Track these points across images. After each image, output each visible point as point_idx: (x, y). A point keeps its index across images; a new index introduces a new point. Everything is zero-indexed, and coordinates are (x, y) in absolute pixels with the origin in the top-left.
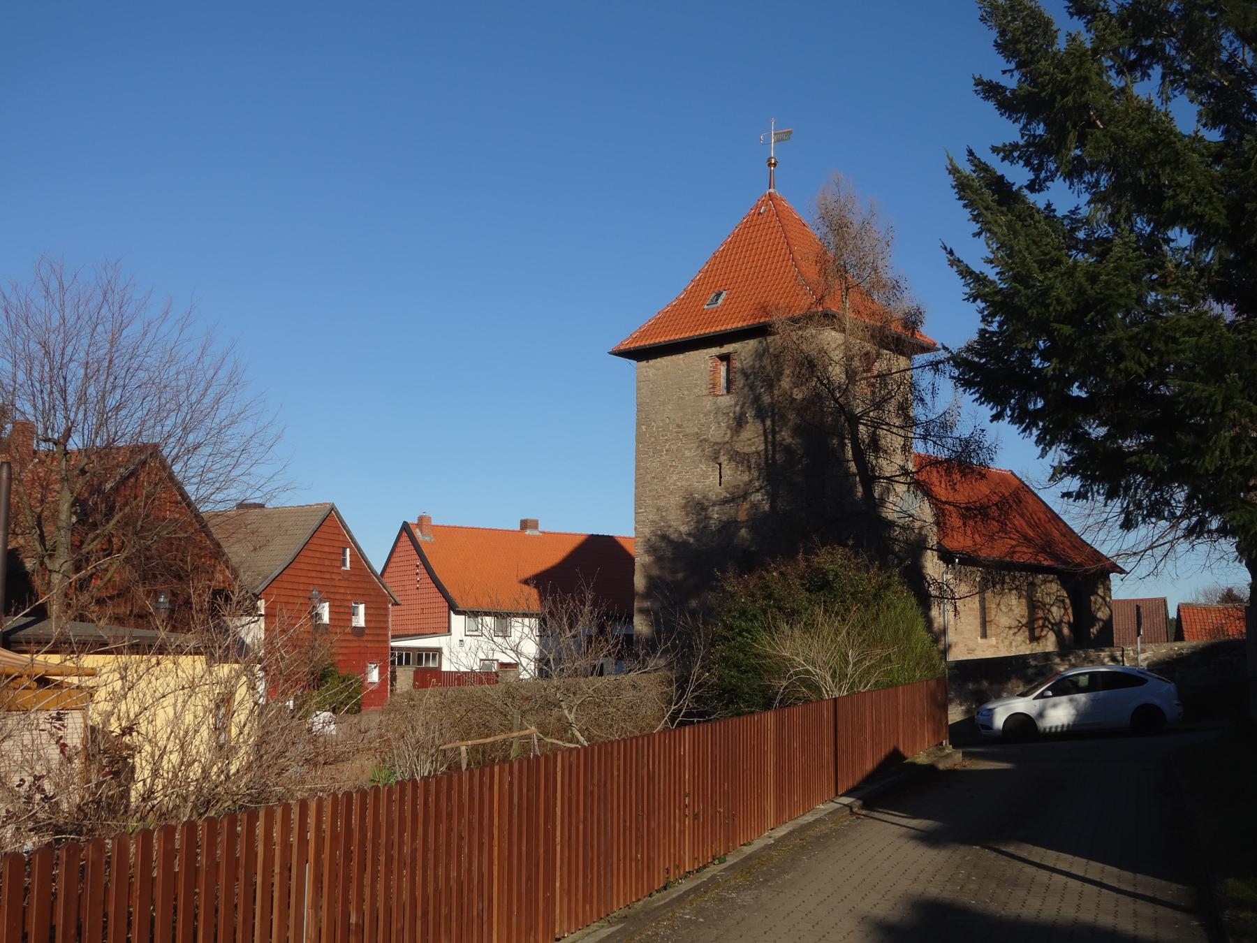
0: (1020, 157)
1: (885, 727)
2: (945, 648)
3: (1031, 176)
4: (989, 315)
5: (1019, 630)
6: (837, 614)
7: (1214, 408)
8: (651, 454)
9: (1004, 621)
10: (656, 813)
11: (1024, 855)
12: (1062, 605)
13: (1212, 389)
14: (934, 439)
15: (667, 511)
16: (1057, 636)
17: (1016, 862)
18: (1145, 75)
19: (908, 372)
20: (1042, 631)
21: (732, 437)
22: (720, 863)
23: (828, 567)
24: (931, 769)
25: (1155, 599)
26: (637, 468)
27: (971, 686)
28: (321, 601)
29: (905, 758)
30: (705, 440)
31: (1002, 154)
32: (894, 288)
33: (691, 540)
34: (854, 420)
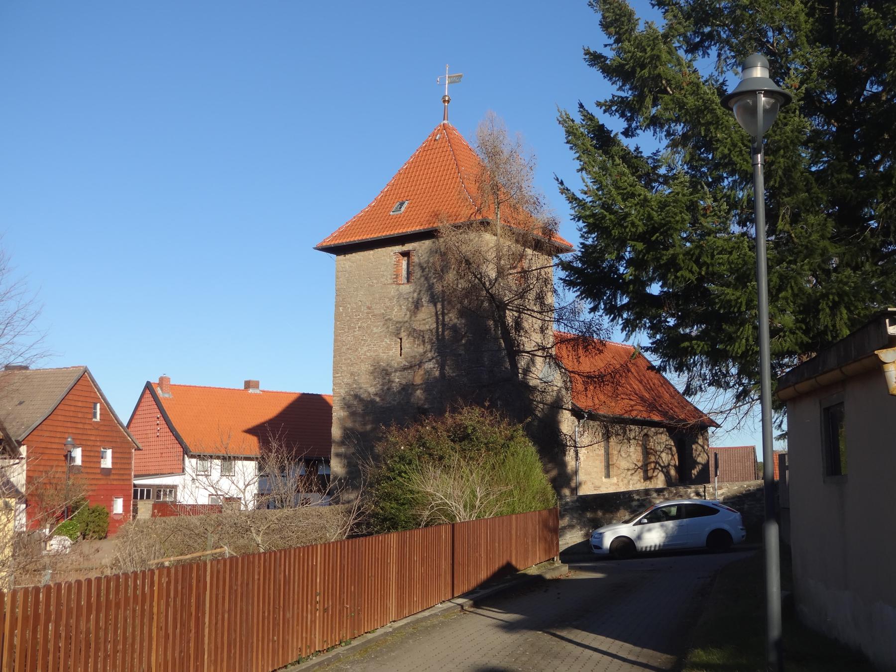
0: (616, 111)
1: (499, 546)
2: (576, 485)
3: (625, 125)
4: (586, 233)
5: (636, 471)
6: (471, 458)
7: (740, 307)
8: (346, 330)
9: (624, 464)
10: (291, 607)
11: (571, 636)
12: (670, 452)
13: (738, 294)
14: (566, 322)
15: (358, 375)
16: (666, 476)
17: (564, 642)
18: (705, 54)
19: (542, 271)
20: (654, 472)
21: (410, 318)
22: (346, 645)
23: (468, 423)
24: (538, 580)
25: (747, 447)
26: (336, 341)
27: (589, 515)
28: (75, 446)
29: (518, 571)
30: (390, 319)
31: (604, 108)
32: (534, 203)
33: (378, 399)
34: (502, 307)
